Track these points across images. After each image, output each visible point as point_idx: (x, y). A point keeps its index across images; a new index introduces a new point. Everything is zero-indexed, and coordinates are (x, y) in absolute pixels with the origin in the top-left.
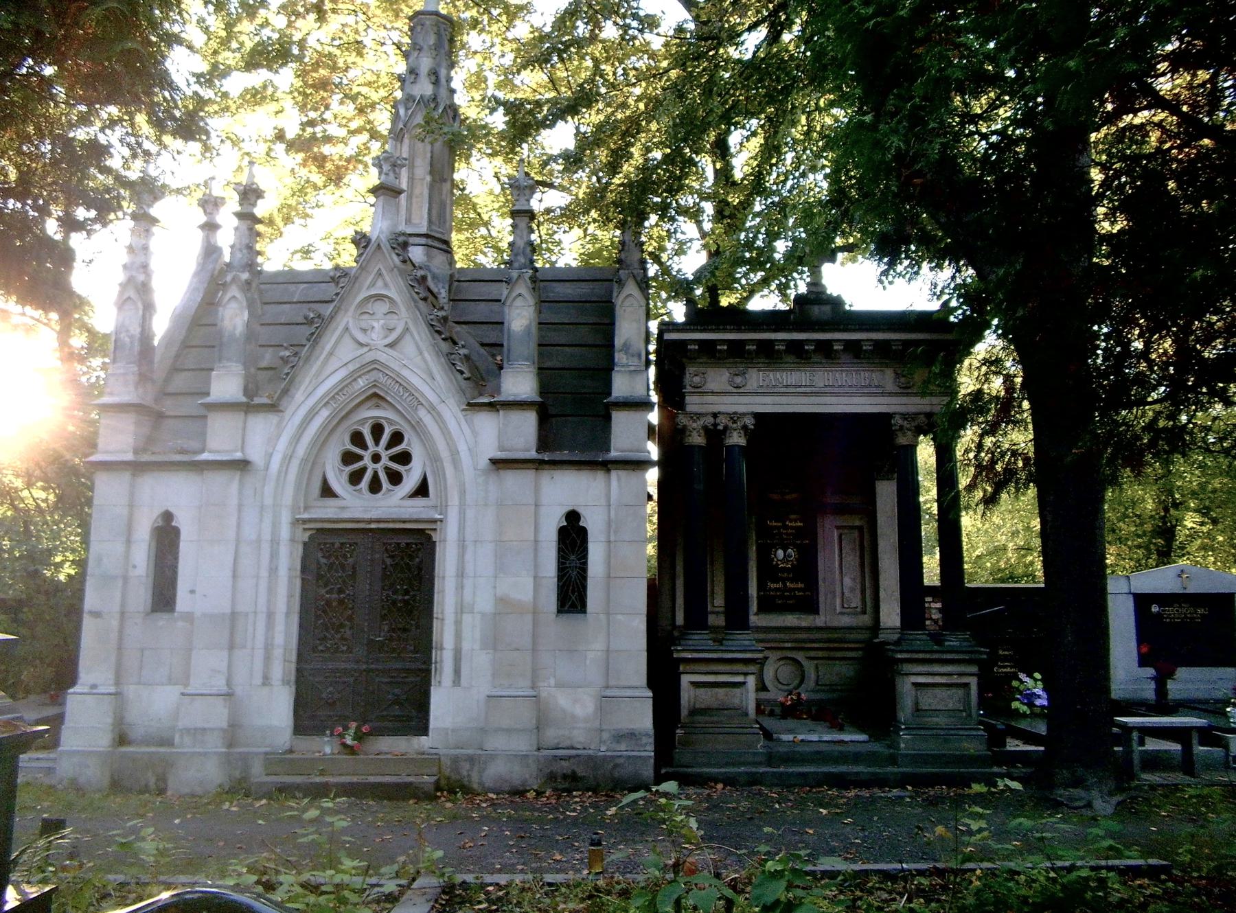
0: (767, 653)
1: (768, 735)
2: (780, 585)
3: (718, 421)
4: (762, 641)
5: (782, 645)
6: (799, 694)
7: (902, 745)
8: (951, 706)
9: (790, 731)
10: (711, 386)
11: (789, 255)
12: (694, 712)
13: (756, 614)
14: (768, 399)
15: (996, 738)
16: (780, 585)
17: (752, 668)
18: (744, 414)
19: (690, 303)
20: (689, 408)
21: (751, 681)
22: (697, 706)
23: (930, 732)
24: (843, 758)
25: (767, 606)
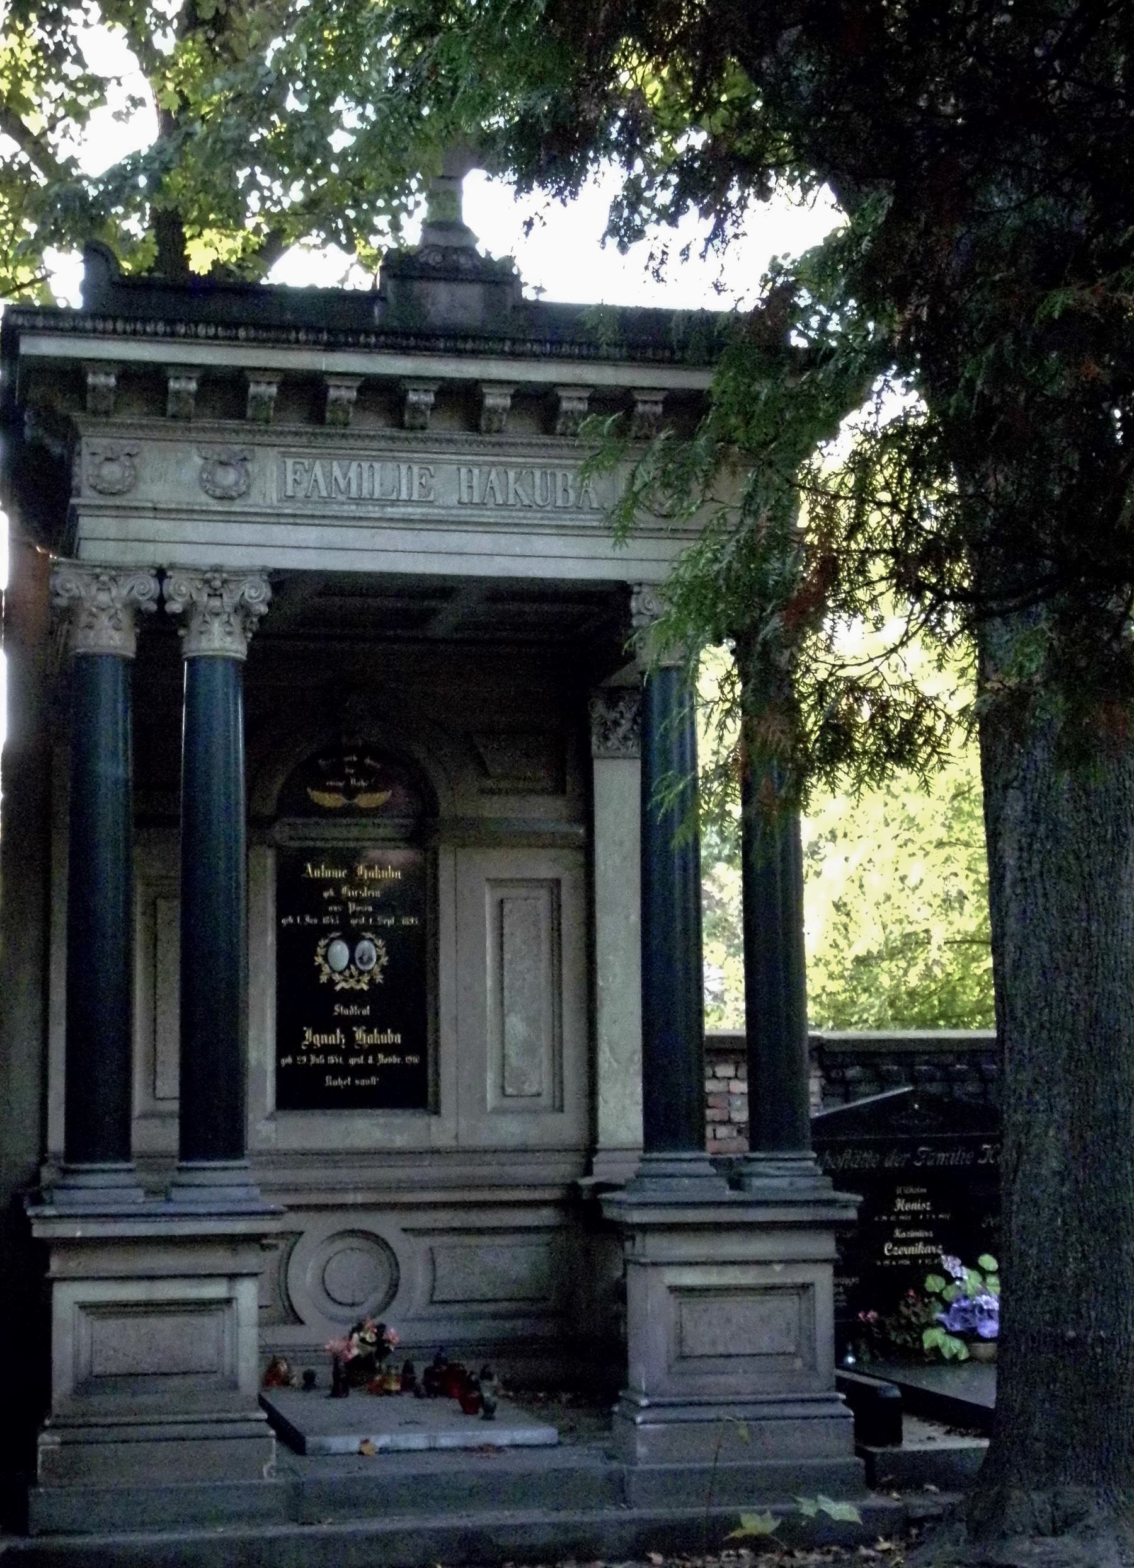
0: (293, 1221)
1: (291, 1439)
2: (337, 1038)
3: (169, 587)
4: (285, 1189)
5: (339, 1199)
6: (381, 1329)
7: (641, 1450)
8: (764, 1344)
9: (351, 1427)
10: (154, 491)
11: (371, 142)
12: (90, 1384)
13: (271, 1118)
14: (310, 534)
15: (875, 1419)
16: (337, 1038)
17: (249, 1260)
18: (241, 573)
19: (98, 255)
20: (91, 551)
21: (247, 1294)
22: (98, 1369)
23: (712, 1413)
24: (491, 1490)
25: (299, 1091)
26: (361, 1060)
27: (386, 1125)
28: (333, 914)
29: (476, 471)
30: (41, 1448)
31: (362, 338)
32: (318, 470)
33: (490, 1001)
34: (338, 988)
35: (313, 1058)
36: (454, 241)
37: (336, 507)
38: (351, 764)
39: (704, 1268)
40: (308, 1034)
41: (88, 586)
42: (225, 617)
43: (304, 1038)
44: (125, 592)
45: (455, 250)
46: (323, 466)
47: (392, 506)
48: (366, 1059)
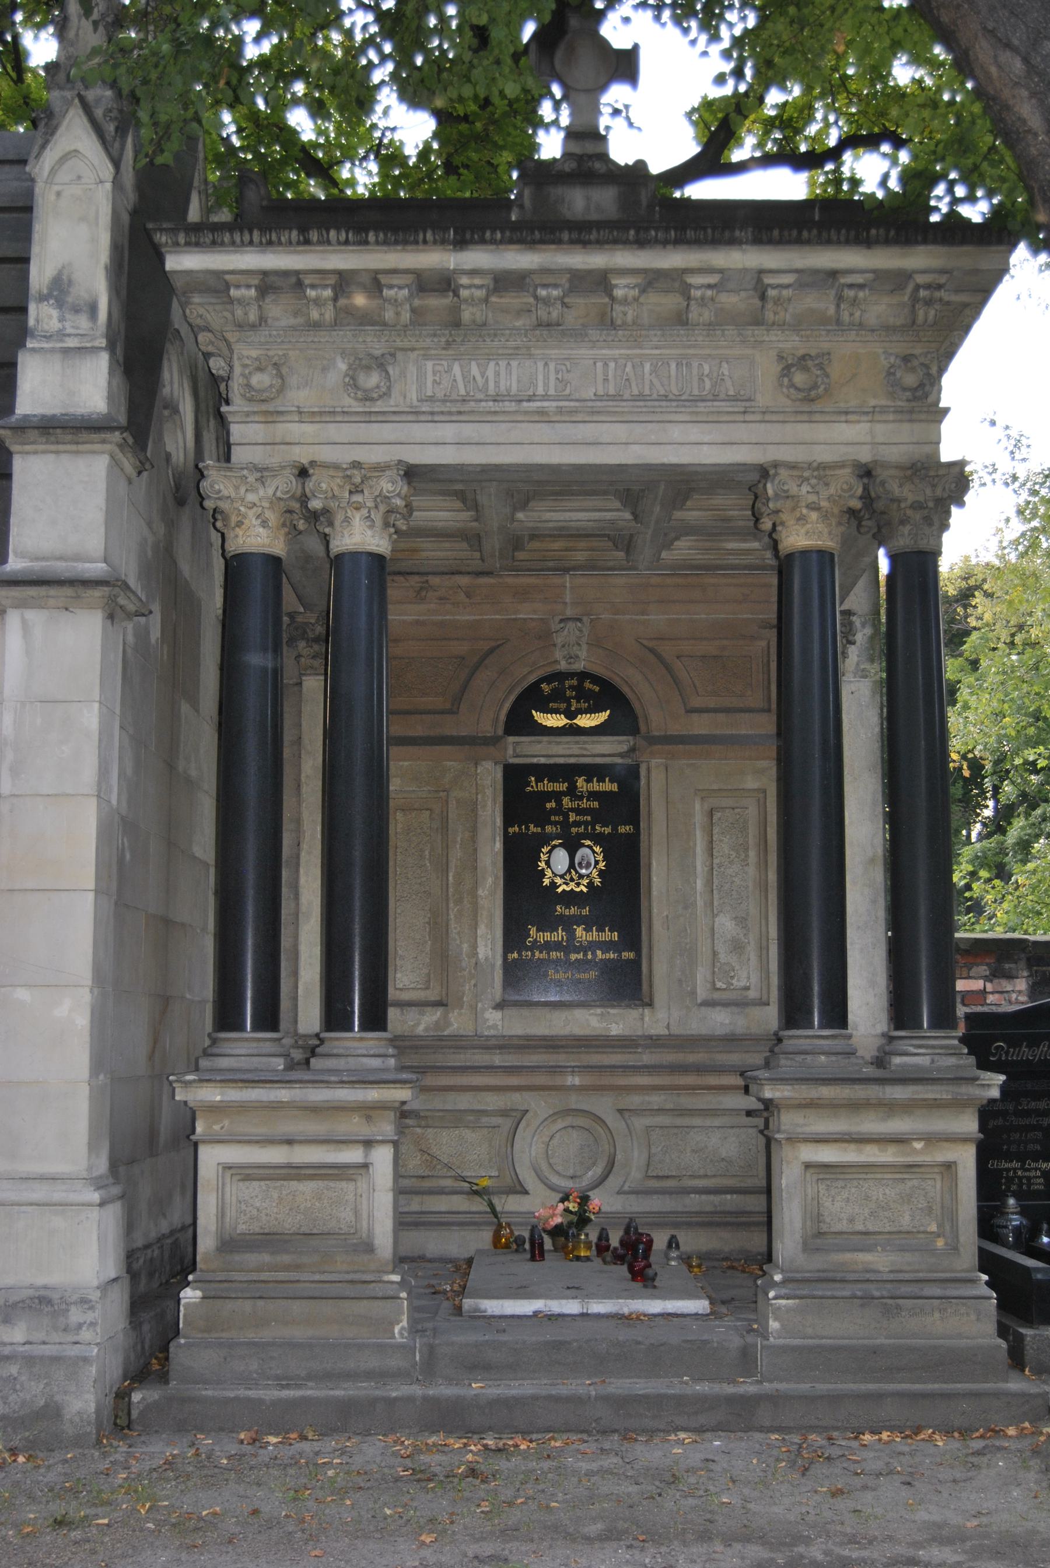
0: (517, 1099)
3: (310, 484)
6: (584, 1200)
7: (774, 1325)
12: (229, 1244)
13: (500, 1006)
14: (447, 431)
18: (380, 468)
26: (580, 956)
27: (602, 1014)
28: (556, 823)
29: (612, 365)
30: (183, 1302)
31: (488, 234)
32: (457, 369)
33: (700, 903)
34: (560, 890)
35: (537, 953)
36: (590, 148)
37: (472, 404)
38: (571, 687)
39: (838, 1145)
40: (533, 931)
41: (237, 488)
42: (365, 512)
43: (529, 936)
44: (270, 491)
45: (590, 157)
46: (461, 366)
47: (529, 401)
48: (585, 955)
